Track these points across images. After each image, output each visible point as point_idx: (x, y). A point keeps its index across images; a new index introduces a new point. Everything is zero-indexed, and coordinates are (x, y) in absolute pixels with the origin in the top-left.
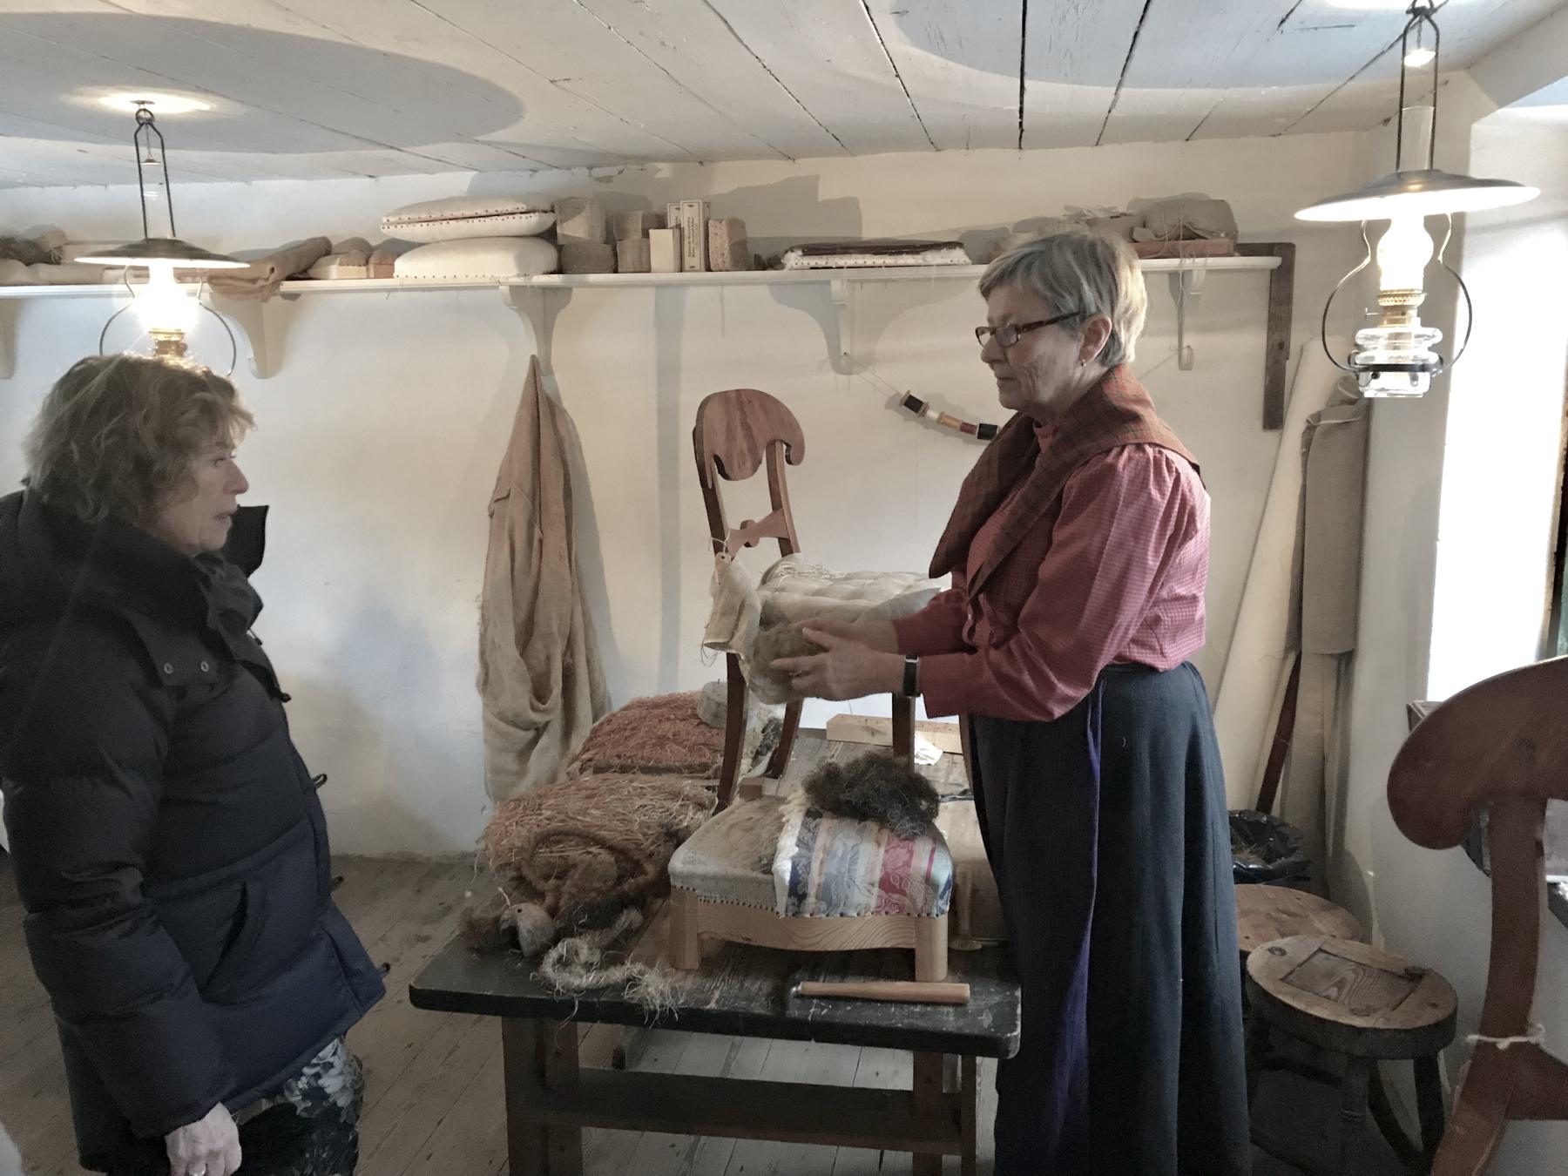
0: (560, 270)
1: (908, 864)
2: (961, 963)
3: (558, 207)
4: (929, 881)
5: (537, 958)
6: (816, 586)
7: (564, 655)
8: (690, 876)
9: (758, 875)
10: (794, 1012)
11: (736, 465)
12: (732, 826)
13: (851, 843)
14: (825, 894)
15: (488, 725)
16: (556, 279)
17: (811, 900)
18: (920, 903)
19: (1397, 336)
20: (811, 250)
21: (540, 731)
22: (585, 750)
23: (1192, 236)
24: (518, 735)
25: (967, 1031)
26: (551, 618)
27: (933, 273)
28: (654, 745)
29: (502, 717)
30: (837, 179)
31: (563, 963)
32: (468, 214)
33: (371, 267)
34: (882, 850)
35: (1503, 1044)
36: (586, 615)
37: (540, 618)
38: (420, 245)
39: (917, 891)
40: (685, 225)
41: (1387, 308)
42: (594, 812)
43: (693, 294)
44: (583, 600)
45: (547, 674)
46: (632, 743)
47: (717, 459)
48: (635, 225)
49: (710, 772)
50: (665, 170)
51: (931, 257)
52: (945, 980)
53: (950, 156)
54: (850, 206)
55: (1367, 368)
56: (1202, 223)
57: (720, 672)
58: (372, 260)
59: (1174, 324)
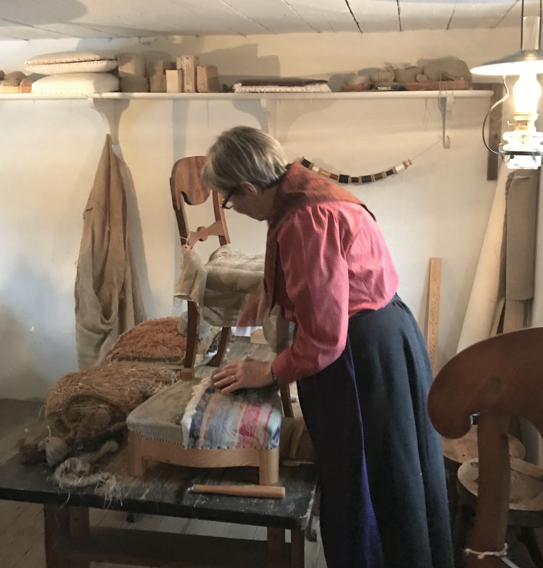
0: (120, 90)
1: (255, 420)
2: (287, 473)
3: (119, 58)
4: (267, 429)
5: (53, 469)
6: (237, 263)
7: (120, 294)
8: (136, 426)
9: (174, 425)
10: (186, 502)
11: (194, 197)
12: (170, 396)
13: (225, 408)
14: (209, 436)
15: (78, 331)
16: (116, 95)
17: (202, 440)
18: (261, 441)
19: (523, 136)
20: (246, 83)
21: (106, 334)
22: (116, 347)
23: (445, 78)
24: (93, 335)
25: (278, 515)
26: (113, 274)
27: (311, 96)
28: (152, 346)
29: (85, 326)
30: (267, 46)
31: (67, 471)
32: (69, 60)
33: (20, 87)
34: (242, 413)
35: (481, 556)
36: (133, 272)
37: (107, 274)
38: (49, 76)
39: (260, 434)
40: (184, 68)
41: (519, 122)
42: (106, 384)
43: (193, 104)
44: (132, 265)
45: (110, 304)
46: (139, 345)
47: (183, 193)
48: (159, 68)
49: (180, 362)
50: (178, 39)
51: (310, 88)
52: (276, 485)
53: (326, 35)
54: (274, 60)
55: (508, 153)
56: (451, 72)
57: (184, 307)
58: (21, 84)
59: (441, 124)
